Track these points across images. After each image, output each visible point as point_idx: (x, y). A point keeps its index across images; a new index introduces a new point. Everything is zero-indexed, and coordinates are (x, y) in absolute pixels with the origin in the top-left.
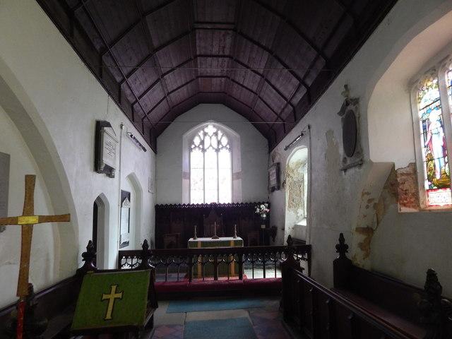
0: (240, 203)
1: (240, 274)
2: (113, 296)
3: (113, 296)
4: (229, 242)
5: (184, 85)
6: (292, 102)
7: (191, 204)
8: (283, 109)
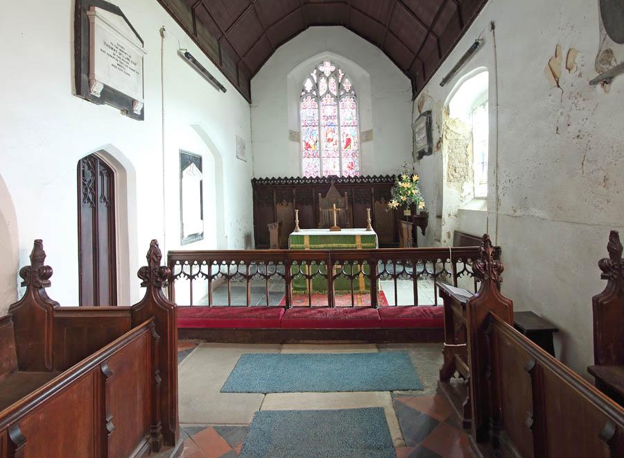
0: (358, 176)
1: (374, 293)
8: (439, 12)
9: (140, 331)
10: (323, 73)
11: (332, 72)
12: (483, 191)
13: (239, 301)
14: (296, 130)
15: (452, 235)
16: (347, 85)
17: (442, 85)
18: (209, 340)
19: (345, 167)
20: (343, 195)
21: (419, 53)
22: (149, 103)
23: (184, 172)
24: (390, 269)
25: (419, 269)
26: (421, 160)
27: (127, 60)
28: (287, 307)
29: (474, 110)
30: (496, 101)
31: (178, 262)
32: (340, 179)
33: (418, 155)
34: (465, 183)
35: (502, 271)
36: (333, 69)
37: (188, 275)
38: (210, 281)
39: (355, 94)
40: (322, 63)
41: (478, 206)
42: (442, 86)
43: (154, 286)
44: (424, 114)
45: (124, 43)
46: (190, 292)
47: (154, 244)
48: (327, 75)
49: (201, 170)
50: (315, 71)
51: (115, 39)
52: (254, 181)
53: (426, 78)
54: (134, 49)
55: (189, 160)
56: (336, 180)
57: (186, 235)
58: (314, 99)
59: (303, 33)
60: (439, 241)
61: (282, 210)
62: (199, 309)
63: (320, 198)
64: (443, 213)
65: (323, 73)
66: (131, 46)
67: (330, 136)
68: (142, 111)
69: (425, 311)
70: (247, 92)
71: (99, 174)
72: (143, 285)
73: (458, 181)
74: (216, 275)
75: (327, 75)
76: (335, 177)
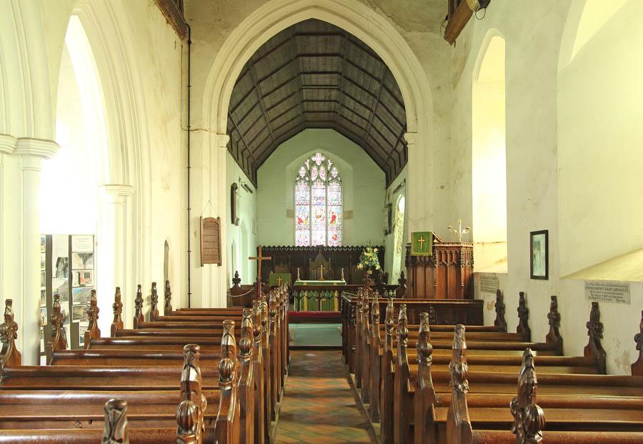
2: (280, 280)
3: (280, 280)
4: (333, 283)
5: (286, 99)
6: (397, 148)
7: (297, 245)
16: (335, 173)
19: (330, 238)
52: (220, 265)
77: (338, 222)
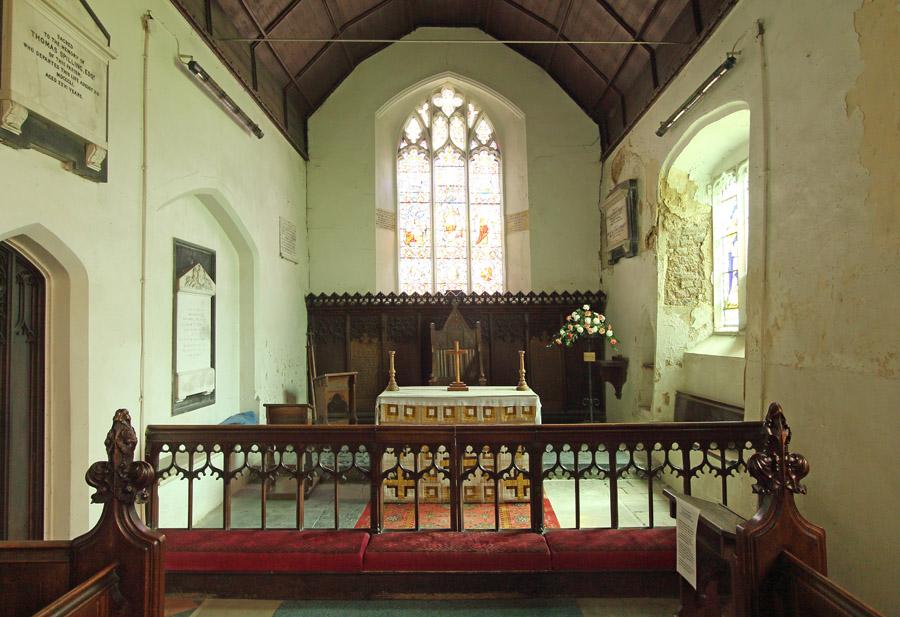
0: (501, 291)
1: (538, 505)
9: (88, 593)
10: (440, 109)
11: (457, 109)
12: (732, 320)
13: (282, 518)
14: (390, 209)
15: (672, 399)
17: (660, 134)
18: (223, 594)
20: (473, 326)
21: (616, 76)
22: (119, 150)
23: (182, 280)
24: (567, 458)
25: (622, 459)
26: (616, 267)
27: (77, 69)
28: (373, 530)
29: (715, 179)
30: (764, 158)
31: (166, 447)
32: (468, 297)
33: (609, 257)
34: (696, 309)
35: (805, 474)
36: (459, 102)
37: (184, 471)
38: (226, 483)
39: (500, 145)
40: (439, 91)
41: (718, 348)
42: (661, 135)
43: (119, 501)
44: (623, 185)
45: (72, 35)
46: (185, 502)
47: (121, 419)
48: (448, 114)
49: (213, 278)
50: (426, 106)
51: (54, 27)
52: (310, 299)
53: (627, 122)
54: (94, 50)
55: (189, 259)
56: (462, 300)
57: (182, 396)
58: (423, 155)
59: (309, 134)
60: (648, 408)
61: (363, 352)
62: (206, 534)
63: (433, 332)
64: (657, 359)
65: (440, 109)
66: (85, 46)
67: (450, 223)
68: (104, 164)
69: (633, 539)
70: (302, 141)
71: (14, 280)
72: (96, 499)
73: (685, 303)
74: (240, 470)
75: (448, 114)
76: (460, 295)
77: (495, 238)
